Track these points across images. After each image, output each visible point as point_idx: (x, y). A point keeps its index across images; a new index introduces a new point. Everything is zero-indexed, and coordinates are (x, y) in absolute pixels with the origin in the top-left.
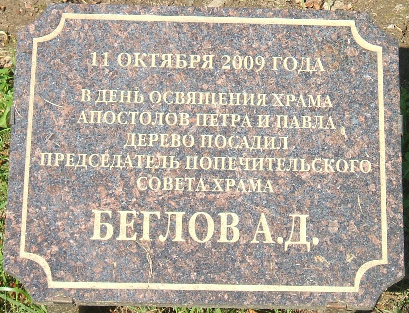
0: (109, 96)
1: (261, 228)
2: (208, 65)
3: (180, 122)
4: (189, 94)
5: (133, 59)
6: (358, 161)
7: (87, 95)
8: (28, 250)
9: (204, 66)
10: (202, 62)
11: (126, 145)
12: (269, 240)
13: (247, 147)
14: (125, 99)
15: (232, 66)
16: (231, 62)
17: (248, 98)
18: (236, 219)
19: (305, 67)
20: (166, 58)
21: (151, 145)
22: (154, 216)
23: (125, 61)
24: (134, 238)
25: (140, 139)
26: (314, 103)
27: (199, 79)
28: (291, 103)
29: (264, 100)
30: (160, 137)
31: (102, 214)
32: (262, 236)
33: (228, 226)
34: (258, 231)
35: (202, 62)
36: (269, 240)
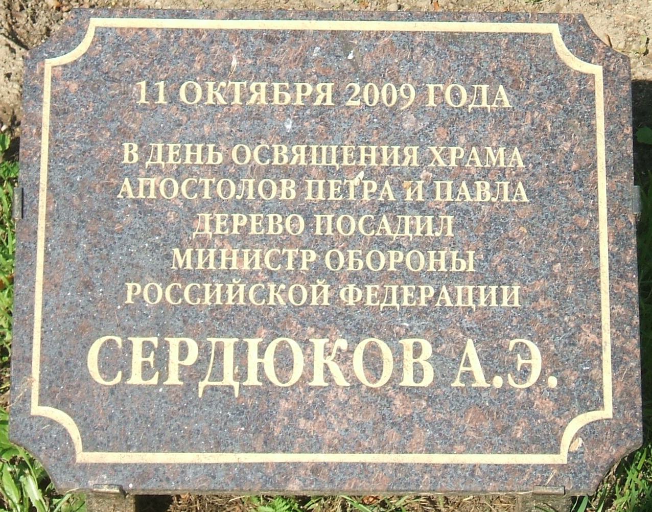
0: (167, 153)
1: (467, 363)
2: (324, 100)
3: (281, 194)
4: (406, 150)
5: (205, 90)
6: (213, 180)
7: (132, 152)
8: (42, 403)
9: (318, 102)
10: (314, 97)
11: (196, 232)
12: (480, 380)
13: (389, 233)
14: (193, 157)
15: (362, 101)
16: (361, 94)
17: (391, 155)
18: (427, 348)
19: (479, 101)
20: (258, 88)
21: (235, 231)
22: (149, 344)
23: (191, 94)
24: (154, 381)
25: (219, 224)
26: (494, 160)
27: (320, 123)
28: (459, 162)
29: (415, 156)
30: (249, 218)
31: (143, 343)
32: (468, 377)
33: (182, 363)
34: (462, 369)
35: (314, 97)
36: (480, 380)
